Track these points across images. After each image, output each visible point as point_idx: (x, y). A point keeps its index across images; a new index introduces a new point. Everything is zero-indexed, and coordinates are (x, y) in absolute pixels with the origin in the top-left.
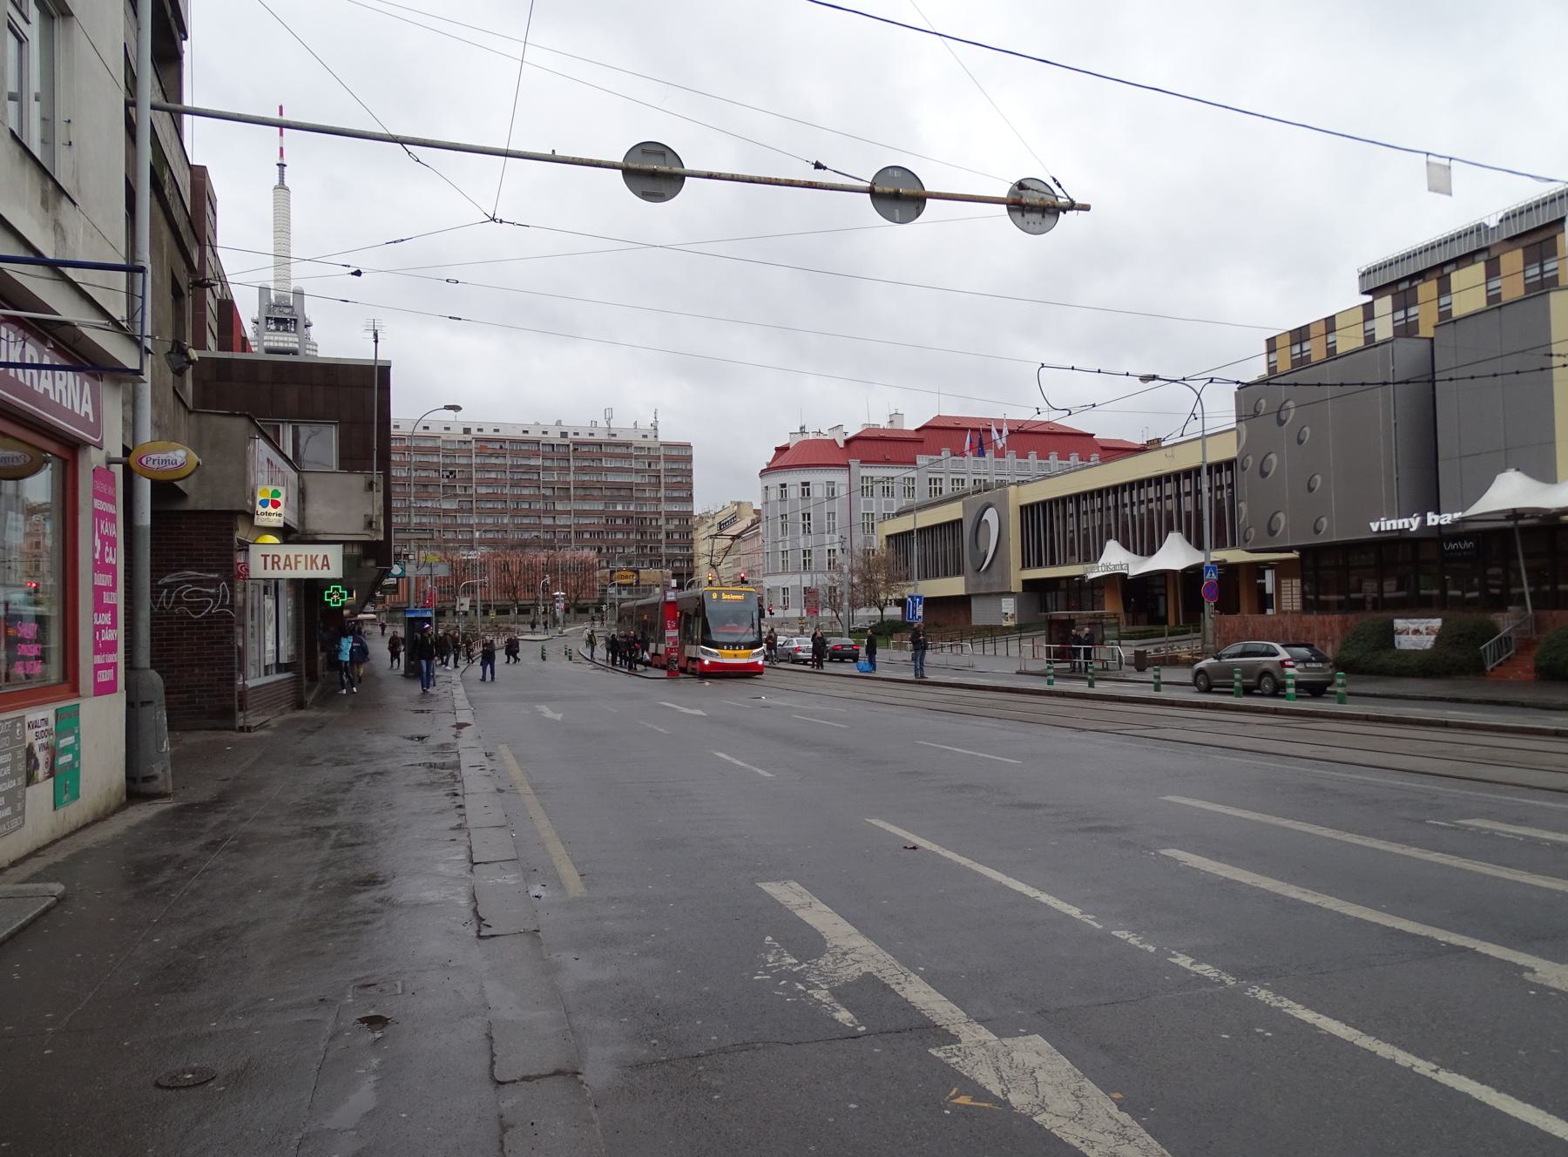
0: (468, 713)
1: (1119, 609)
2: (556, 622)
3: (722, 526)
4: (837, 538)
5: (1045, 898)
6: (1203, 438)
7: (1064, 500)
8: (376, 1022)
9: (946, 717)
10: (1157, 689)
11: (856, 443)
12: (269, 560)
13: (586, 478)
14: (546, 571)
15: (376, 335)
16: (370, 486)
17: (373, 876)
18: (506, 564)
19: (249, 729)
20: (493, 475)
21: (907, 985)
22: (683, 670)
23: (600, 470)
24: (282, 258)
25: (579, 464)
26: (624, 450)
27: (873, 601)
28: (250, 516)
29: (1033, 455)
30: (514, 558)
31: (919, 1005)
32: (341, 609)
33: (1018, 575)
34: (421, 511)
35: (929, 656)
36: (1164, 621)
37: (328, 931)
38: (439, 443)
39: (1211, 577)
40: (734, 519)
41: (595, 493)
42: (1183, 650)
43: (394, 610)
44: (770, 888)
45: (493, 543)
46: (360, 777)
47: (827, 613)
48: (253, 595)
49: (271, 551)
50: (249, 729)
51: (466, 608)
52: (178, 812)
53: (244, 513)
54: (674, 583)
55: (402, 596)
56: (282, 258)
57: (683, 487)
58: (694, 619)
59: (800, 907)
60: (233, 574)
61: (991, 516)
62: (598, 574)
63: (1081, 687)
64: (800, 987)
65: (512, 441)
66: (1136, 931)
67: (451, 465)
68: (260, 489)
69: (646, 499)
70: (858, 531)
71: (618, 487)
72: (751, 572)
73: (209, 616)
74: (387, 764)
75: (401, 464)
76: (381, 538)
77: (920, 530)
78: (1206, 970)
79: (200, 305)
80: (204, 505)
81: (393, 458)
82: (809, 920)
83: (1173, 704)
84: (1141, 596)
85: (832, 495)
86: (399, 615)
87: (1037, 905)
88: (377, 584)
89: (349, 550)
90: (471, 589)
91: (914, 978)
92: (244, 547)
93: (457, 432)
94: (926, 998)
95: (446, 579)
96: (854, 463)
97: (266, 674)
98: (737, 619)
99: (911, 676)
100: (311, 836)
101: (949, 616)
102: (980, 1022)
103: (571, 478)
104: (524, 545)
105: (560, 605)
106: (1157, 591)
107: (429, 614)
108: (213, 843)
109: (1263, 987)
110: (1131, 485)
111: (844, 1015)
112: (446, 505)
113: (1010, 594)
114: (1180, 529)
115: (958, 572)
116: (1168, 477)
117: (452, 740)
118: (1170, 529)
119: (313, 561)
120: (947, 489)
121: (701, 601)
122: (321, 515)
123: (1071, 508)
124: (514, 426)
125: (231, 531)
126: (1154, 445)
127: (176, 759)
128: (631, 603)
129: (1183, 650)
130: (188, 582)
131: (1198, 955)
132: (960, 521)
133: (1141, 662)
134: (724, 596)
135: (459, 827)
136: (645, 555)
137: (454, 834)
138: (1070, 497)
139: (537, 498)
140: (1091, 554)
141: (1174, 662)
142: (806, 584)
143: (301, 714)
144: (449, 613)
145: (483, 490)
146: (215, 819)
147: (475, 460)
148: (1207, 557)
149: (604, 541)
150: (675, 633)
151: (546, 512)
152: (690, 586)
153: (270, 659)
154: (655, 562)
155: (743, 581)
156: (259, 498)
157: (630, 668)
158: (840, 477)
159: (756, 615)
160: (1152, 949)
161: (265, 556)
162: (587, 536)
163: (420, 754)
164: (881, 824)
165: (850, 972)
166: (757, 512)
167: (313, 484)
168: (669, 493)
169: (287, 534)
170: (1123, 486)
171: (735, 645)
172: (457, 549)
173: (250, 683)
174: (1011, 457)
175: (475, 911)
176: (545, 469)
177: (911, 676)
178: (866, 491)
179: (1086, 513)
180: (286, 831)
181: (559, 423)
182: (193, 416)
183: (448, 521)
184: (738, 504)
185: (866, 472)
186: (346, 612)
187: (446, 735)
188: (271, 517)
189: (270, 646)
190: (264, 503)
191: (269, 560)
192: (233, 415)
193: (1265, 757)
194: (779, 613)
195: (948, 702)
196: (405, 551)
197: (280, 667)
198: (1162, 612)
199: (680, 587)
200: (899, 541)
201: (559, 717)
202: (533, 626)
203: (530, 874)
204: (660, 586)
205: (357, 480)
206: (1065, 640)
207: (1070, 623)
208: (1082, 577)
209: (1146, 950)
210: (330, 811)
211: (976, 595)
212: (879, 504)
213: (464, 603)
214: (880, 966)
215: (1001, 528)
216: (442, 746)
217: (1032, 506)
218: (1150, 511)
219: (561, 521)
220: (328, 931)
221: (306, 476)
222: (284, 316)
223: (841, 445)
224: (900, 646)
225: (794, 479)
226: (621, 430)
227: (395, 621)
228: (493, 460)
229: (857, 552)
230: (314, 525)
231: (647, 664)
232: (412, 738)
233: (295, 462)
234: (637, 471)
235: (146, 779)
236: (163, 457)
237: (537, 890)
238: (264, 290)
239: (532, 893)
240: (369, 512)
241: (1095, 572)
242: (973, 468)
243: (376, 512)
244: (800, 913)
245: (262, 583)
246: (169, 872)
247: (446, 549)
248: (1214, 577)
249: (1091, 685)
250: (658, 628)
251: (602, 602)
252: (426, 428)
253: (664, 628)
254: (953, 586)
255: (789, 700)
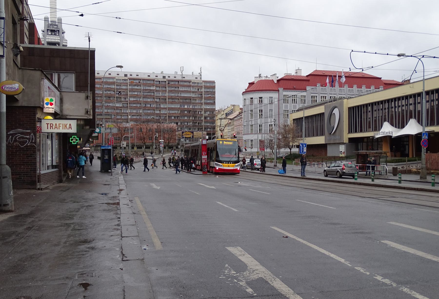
0: (124, 185)
1: (389, 150)
2: (160, 152)
3: (227, 115)
4: (273, 120)
5: (332, 255)
6: (424, 80)
7: (367, 105)
8: (86, 286)
9: (310, 191)
10: (400, 182)
11: (282, 81)
12: (49, 125)
13: (173, 95)
14: (157, 132)
15: (89, 39)
16: (87, 97)
17: (86, 240)
18: (141, 129)
19: (42, 189)
20: (136, 93)
21: (274, 281)
22: (208, 172)
23: (178, 92)
24: (53, 8)
25: (170, 89)
26: (188, 84)
27: (287, 146)
28: (42, 108)
29: (355, 87)
30: (144, 126)
31: (277, 288)
32: (77, 145)
33: (347, 136)
34: (107, 107)
35: (307, 168)
36: (408, 155)
37: (70, 257)
38: (115, 80)
39: (425, 137)
40: (231, 112)
41: (176, 101)
42: (414, 168)
43: (97, 146)
44: (230, 249)
45: (136, 120)
46: (82, 207)
47: (268, 150)
48: (43, 138)
49: (50, 122)
50: (42, 189)
51: (125, 146)
52: (17, 217)
53: (40, 107)
54: (207, 137)
55: (99, 141)
56: (53, 8)
57: (212, 99)
58: (212, 151)
59: (240, 255)
60: (35, 130)
61: (336, 111)
62: (177, 133)
63: (369, 181)
64: (235, 281)
65: (143, 80)
66: (364, 268)
67: (120, 89)
68: (45, 98)
69: (196, 103)
70: (282, 117)
71: (186, 98)
72: (238, 133)
73: (27, 146)
74: (92, 203)
75: (100, 89)
76: (91, 118)
77: (307, 118)
78: (387, 281)
79: (22, 26)
80: (25, 104)
81: (96, 86)
82: (243, 260)
83: (404, 188)
84: (399, 145)
85: (271, 103)
86: (99, 148)
87: (329, 257)
88: (90, 136)
89: (79, 122)
90: (126, 139)
91: (277, 279)
92: (40, 120)
93: (122, 76)
94: (280, 286)
95: (117, 134)
96: (281, 89)
97: (48, 169)
98: (230, 151)
99: (299, 175)
100: (64, 226)
101: (317, 152)
102: (298, 294)
103: (167, 95)
104: (148, 121)
105: (162, 145)
106: (405, 143)
107: (110, 148)
108: (29, 228)
109: (406, 287)
110: (395, 99)
111: (250, 290)
112: (118, 105)
113: (343, 143)
114: (415, 118)
115: (322, 134)
116: (410, 96)
117: (117, 195)
118: (411, 117)
119: (66, 126)
120: (319, 100)
121: (216, 144)
122: (68, 109)
123: (370, 108)
124: (144, 74)
125: (35, 114)
126: (407, 82)
127: (15, 199)
128: (189, 145)
129: (414, 168)
130: (19, 133)
131: (385, 276)
132: (324, 113)
133: (395, 172)
134: (225, 143)
135: (118, 225)
136: (196, 126)
137: (117, 227)
138: (369, 104)
139: (153, 102)
140: (377, 128)
141: (409, 172)
142: (260, 138)
143: (61, 184)
144: (119, 148)
145: (132, 99)
146: (30, 220)
147: (129, 87)
148: (424, 129)
149: (180, 120)
150: (206, 157)
151: (157, 108)
152: (213, 138)
153: (49, 163)
154: (200, 129)
155: (235, 137)
156: (45, 102)
157: (188, 170)
158: (275, 95)
159: (237, 151)
160: (368, 273)
161: (48, 124)
162: (173, 118)
163: (105, 200)
164: (276, 229)
165: (254, 277)
166: (241, 109)
167: (66, 97)
168: (206, 101)
169: (55, 116)
170: (392, 100)
171: (228, 162)
172: (121, 122)
173: (42, 172)
174: (346, 86)
175: (122, 252)
176: (156, 91)
177: (299, 175)
178: (285, 101)
179: (376, 111)
180: (55, 224)
181: (162, 73)
182: (20, 70)
183: (118, 111)
184: (234, 106)
185: (285, 93)
186: (78, 147)
187: (115, 193)
188: (49, 109)
189: (49, 158)
190: (47, 104)
191: (49, 125)
192: (35, 70)
193: (434, 209)
194: (249, 150)
195: (313, 186)
196: (101, 123)
197: (53, 167)
198: (407, 152)
199: (210, 138)
200: (298, 121)
201: (159, 188)
202: (152, 153)
203: (142, 241)
204: (201, 138)
205: (82, 95)
206: (364, 162)
207: (366, 156)
208: (373, 137)
209: (366, 274)
210: (71, 218)
211: (329, 144)
212: (291, 106)
213: (124, 144)
214: (265, 275)
215: (341, 117)
216: (113, 197)
217: (353, 107)
218: (403, 110)
219: (163, 112)
220: (70, 257)
221: (62, 93)
222: (54, 29)
223: (276, 82)
224: (297, 164)
225: (256, 96)
226: (187, 75)
227: (98, 150)
228: (136, 87)
229: (281, 126)
230: (66, 112)
231: (194, 169)
232: (103, 194)
233: (59, 88)
234: (193, 92)
235: (5, 205)
236: (10, 86)
237: (145, 247)
238: (46, 19)
239: (143, 248)
240: (87, 107)
241: (379, 135)
242: (329, 92)
243: (90, 108)
244: (240, 257)
245: (46, 134)
246: (14, 237)
247: (117, 122)
248: (426, 137)
249: (373, 181)
250: (199, 155)
251: (178, 144)
252: (110, 74)
253: (201, 155)
254: (320, 140)
255: (247, 183)
